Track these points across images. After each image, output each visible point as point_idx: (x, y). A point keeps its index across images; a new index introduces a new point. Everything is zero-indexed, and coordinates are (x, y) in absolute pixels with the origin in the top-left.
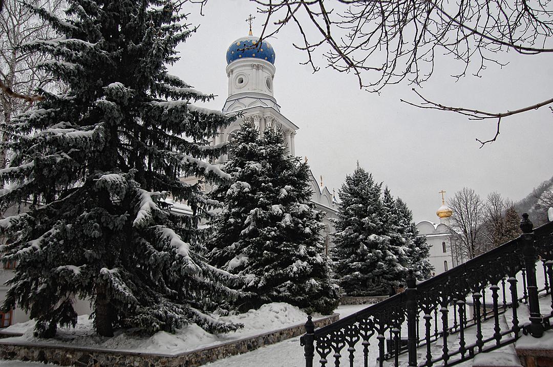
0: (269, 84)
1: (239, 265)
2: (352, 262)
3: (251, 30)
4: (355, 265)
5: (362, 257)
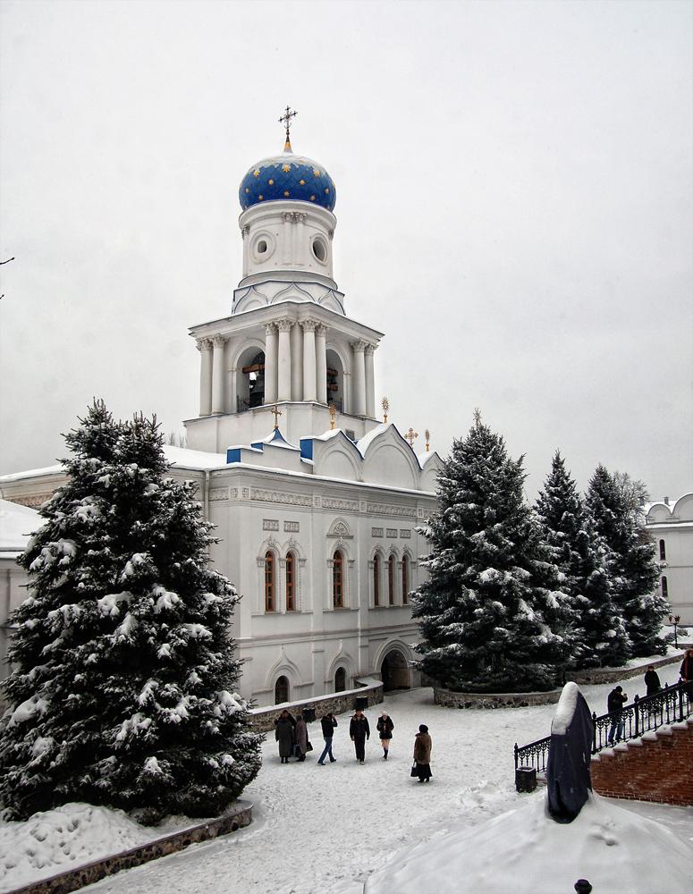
0: (318, 250)
1: (29, 717)
2: (447, 622)
3: (288, 140)
4: (452, 630)
5: (465, 613)
